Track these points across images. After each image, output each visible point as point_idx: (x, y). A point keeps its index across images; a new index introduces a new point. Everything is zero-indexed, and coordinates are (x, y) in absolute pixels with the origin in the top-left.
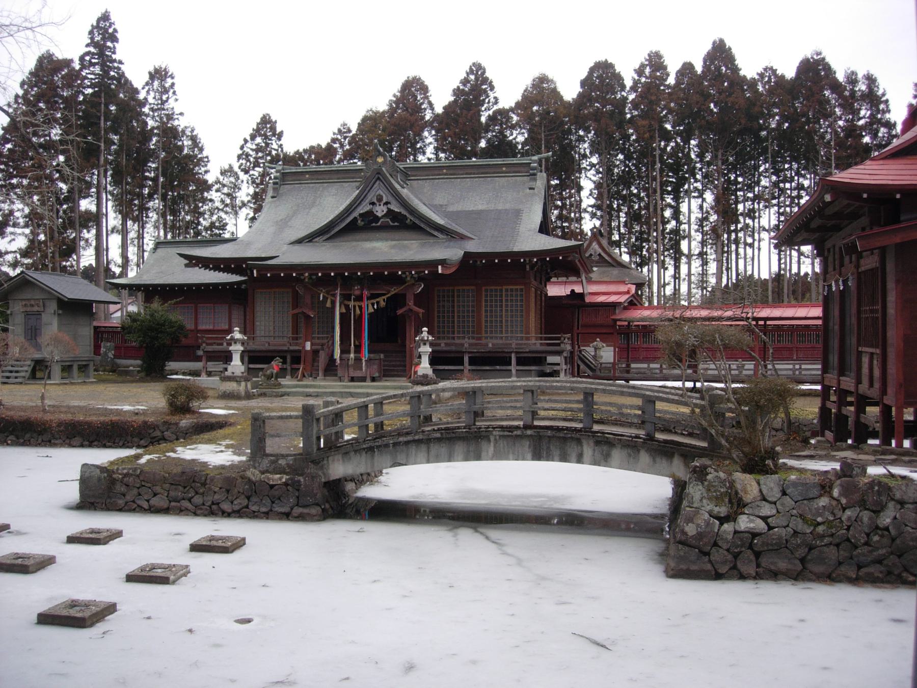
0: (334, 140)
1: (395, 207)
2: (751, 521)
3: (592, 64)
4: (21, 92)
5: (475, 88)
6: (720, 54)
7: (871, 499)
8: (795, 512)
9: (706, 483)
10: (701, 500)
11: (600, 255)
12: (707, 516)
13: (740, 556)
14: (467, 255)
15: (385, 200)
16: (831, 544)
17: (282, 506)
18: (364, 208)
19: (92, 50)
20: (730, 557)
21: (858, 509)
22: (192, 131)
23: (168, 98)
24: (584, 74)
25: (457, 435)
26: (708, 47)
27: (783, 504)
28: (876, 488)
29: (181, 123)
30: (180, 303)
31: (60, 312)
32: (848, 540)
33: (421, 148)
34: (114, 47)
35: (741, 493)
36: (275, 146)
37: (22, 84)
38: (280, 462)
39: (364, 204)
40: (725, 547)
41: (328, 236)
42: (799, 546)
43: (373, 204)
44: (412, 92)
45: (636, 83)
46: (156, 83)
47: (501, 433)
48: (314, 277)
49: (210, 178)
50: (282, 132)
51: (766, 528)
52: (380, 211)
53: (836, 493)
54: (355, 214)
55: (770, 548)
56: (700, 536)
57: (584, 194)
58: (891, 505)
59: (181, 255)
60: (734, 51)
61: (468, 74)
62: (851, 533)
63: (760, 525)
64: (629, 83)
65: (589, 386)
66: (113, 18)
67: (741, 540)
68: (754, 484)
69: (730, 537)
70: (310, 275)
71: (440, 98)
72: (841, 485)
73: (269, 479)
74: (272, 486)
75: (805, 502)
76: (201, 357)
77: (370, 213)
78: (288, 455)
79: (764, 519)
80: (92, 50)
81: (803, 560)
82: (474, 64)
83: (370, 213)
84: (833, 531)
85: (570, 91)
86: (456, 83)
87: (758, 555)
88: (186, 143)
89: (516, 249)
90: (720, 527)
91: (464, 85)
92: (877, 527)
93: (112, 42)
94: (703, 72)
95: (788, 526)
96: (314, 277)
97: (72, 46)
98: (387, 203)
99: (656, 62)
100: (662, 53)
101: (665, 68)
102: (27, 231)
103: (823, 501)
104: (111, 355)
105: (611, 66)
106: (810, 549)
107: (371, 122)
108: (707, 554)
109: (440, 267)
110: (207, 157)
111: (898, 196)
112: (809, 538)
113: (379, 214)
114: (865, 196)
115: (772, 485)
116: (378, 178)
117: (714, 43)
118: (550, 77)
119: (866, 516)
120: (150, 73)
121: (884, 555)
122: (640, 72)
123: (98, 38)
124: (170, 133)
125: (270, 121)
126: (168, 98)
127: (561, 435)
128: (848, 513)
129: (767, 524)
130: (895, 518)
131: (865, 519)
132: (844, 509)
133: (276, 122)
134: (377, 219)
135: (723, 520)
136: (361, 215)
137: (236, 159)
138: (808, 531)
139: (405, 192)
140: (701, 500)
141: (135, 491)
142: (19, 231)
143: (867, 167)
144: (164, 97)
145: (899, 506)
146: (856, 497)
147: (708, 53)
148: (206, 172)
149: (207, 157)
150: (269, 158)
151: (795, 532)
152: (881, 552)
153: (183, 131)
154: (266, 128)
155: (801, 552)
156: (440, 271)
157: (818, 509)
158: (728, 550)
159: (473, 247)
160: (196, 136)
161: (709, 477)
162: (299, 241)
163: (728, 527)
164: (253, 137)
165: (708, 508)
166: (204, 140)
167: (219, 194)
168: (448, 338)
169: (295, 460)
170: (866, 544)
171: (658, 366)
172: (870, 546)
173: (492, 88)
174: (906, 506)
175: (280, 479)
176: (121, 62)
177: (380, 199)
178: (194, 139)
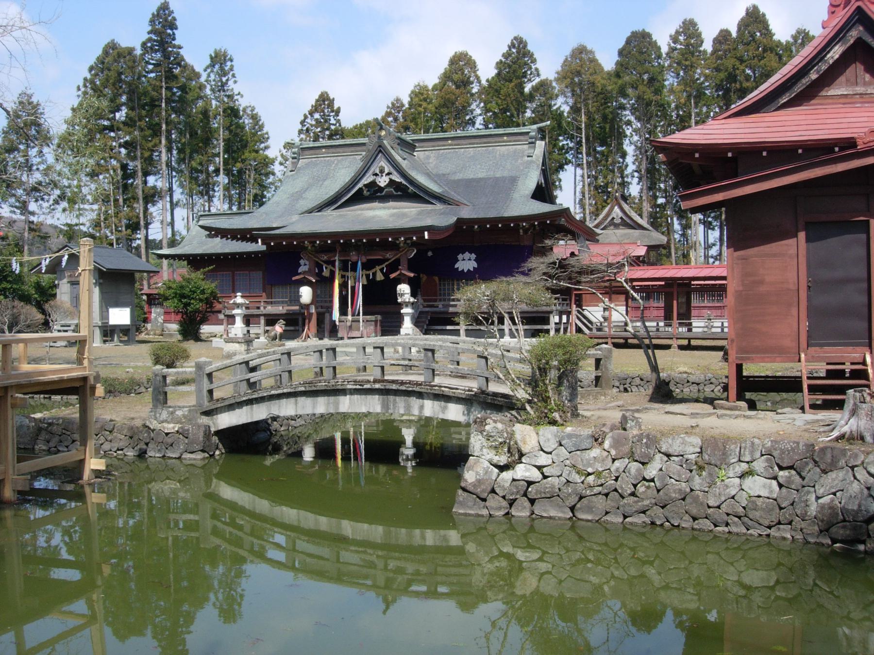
0: (388, 114)
1: (397, 178)
2: (527, 470)
3: (629, 34)
4: (89, 77)
5: (517, 60)
6: (754, 19)
7: (639, 451)
8: (568, 462)
9: (485, 433)
10: (481, 450)
11: (621, 218)
12: (487, 464)
13: (515, 503)
14: (460, 221)
15: (386, 171)
16: (600, 493)
17: (174, 452)
18: (367, 179)
19: (154, 37)
20: (505, 504)
21: (627, 460)
22: (252, 110)
23: (227, 80)
24: (621, 43)
25: (318, 388)
26: (742, 14)
27: (557, 455)
28: (645, 441)
29: (242, 103)
30: (212, 271)
31: (101, 281)
32: (616, 490)
33: (470, 119)
34: (174, 34)
35: (520, 444)
36: (333, 121)
37: (91, 69)
38: (177, 413)
39: (368, 175)
40: (501, 495)
41: (336, 206)
42: (570, 495)
43: (376, 175)
44: (460, 68)
45: (673, 50)
46: (217, 67)
47: (354, 387)
48: (409, 242)
49: (271, 153)
50: (339, 108)
51: (541, 476)
52: (383, 181)
53: (607, 444)
54: (360, 185)
55: (543, 496)
56: (479, 482)
57: (629, 159)
58: (658, 456)
59: (202, 227)
60: (767, 17)
61: (509, 47)
62: (618, 483)
63: (535, 475)
64: (664, 49)
65: (428, 343)
66: (172, 7)
67: (517, 487)
68: (534, 435)
69: (507, 485)
70: (405, 240)
71: (486, 70)
72: (613, 437)
73: (164, 428)
74: (167, 434)
75: (578, 452)
76: (222, 320)
77: (373, 184)
78: (183, 407)
79: (539, 468)
80: (154, 37)
81: (572, 509)
82: (515, 38)
83: (373, 184)
84: (603, 481)
85: (608, 60)
86: (499, 57)
87: (532, 501)
88: (247, 121)
89: (506, 215)
90: (499, 475)
91: (506, 58)
92: (644, 479)
93: (172, 29)
94: (737, 37)
95: (561, 475)
96: (409, 242)
97: (134, 35)
98: (389, 174)
99: (689, 30)
100: (696, 20)
101: (700, 35)
102: (95, 207)
103: (596, 452)
104: (160, 320)
105: (649, 35)
106: (581, 498)
107: (420, 95)
108: (484, 500)
109: (426, 233)
110: (267, 133)
111: (730, 155)
112: (580, 488)
113: (382, 184)
114: (697, 155)
115: (550, 436)
116: (380, 151)
117: (747, 10)
118: (589, 48)
119: (634, 466)
120: (211, 58)
121: (647, 506)
122: (675, 39)
123: (158, 27)
124: (232, 113)
125: (328, 99)
126: (227, 80)
127: (404, 388)
128: (617, 463)
129: (542, 473)
130: (661, 470)
131: (633, 471)
132: (614, 460)
133: (333, 99)
134: (381, 189)
135: (502, 468)
136: (365, 185)
137: (297, 133)
138: (579, 481)
139: (404, 164)
140: (481, 450)
141: (57, 439)
142: (87, 206)
143: (711, 127)
144: (224, 79)
145: (666, 459)
146: (626, 449)
147: (742, 19)
148: (267, 148)
149: (267, 133)
150: (327, 133)
151: (568, 481)
152: (646, 502)
153: (244, 110)
154: (324, 102)
155: (573, 500)
156: (426, 237)
157: (588, 460)
158: (504, 497)
159: (466, 213)
160: (256, 114)
161: (487, 428)
162: (310, 212)
163: (507, 475)
164: (311, 113)
165: (488, 457)
166: (264, 119)
167: (282, 167)
168: (444, 300)
169: (190, 411)
170: (633, 494)
171: (655, 324)
172: (637, 496)
173: (534, 61)
174: (672, 458)
175: (174, 428)
176: (180, 47)
177: (382, 171)
178: (255, 118)
